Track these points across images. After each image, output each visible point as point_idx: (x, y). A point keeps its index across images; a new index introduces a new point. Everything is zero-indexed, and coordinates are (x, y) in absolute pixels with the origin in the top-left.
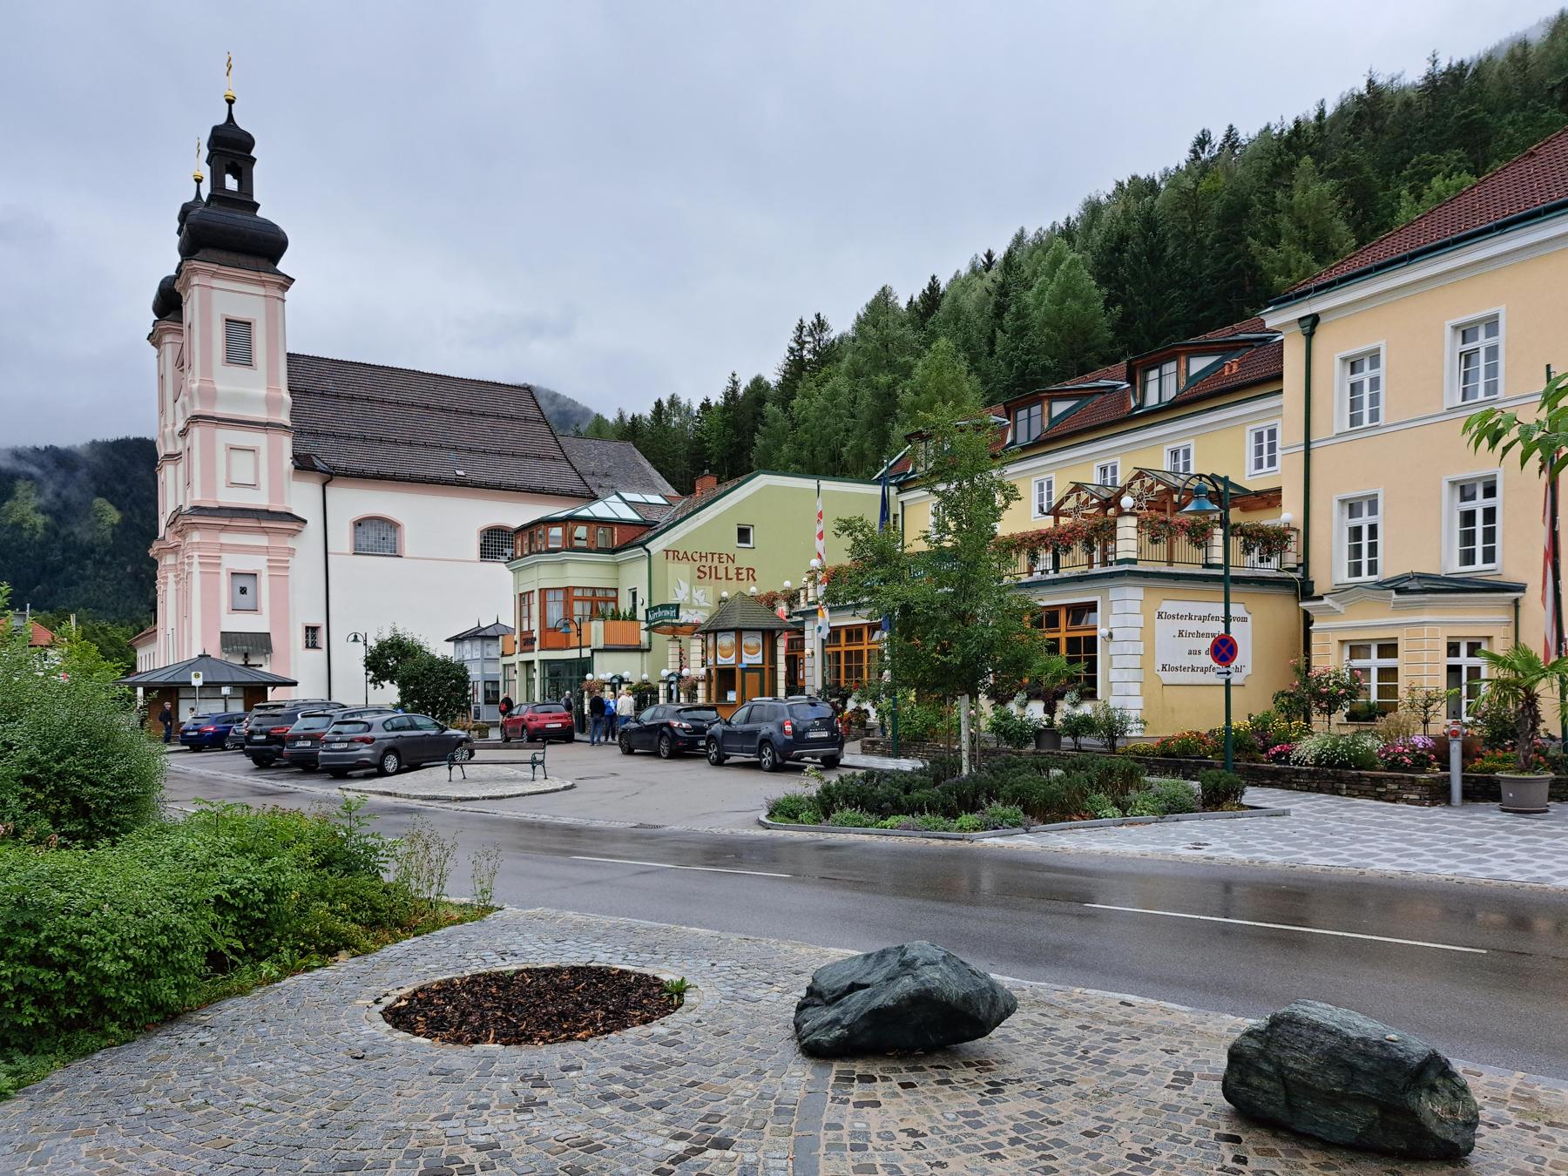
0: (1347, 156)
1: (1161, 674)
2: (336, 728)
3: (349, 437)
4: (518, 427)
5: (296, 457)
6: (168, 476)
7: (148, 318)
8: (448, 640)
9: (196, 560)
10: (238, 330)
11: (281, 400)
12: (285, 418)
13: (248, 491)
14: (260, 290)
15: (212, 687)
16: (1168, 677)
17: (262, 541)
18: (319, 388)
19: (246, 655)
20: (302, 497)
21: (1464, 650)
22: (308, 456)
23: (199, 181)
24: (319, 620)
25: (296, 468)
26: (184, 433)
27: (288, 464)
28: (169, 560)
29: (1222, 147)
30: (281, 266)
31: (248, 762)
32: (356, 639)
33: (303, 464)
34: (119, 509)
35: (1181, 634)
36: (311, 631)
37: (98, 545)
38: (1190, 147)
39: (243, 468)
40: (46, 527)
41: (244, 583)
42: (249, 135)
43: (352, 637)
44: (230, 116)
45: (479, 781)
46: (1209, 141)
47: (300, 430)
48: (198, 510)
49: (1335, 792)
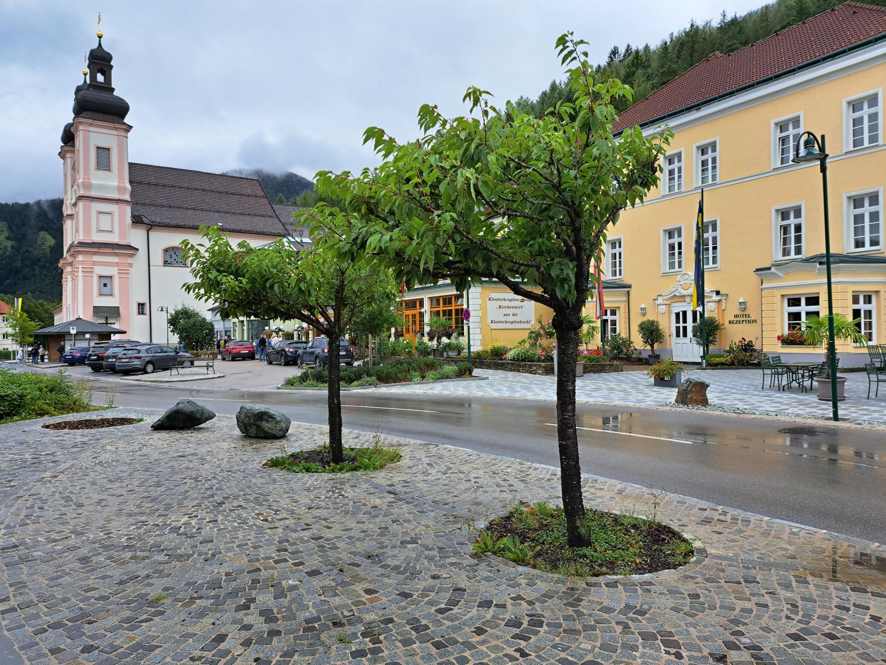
0: (670, 66)
1: (490, 324)
2: (124, 352)
3: (162, 206)
4: (252, 200)
5: (133, 216)
6: (68, 226)
7: (58, 143)
8: (209, 310)
9: (80, 270)
10: (103, 153)
11: (125, 188)
12: (127, 197)
13: (109, 234)
14: (115, 132)
15: (80, 334)
16: (494, 326)
17: (115, 259)
18: (147, 181)
19: (107, 318)
20: (136, 237)
21: (609, 313)
22: (139, 216)
23: (85, 74)
24: (145, 300)
25: (133, 222)
26: (75, 205)
27: (129, 220)
28: (69, 269)
29: (625, 55)
30: (126, 120)
31: (89, 369)
32: (162, 310)
33: (137, 220)
34: (54, 237)
35: (500, 307)
36: (141, 306)
37: (42, 257)
38: (608, 55)
39: (105, 223)
40: (13, 247)
41: (105, 282)
42: (109, 54)
43: (160, 309)
44: (100, 45)
45: (182, 375)
46: (618, 53)
47: (135, 203)
48: (82, 244)
49: (519, 371)
